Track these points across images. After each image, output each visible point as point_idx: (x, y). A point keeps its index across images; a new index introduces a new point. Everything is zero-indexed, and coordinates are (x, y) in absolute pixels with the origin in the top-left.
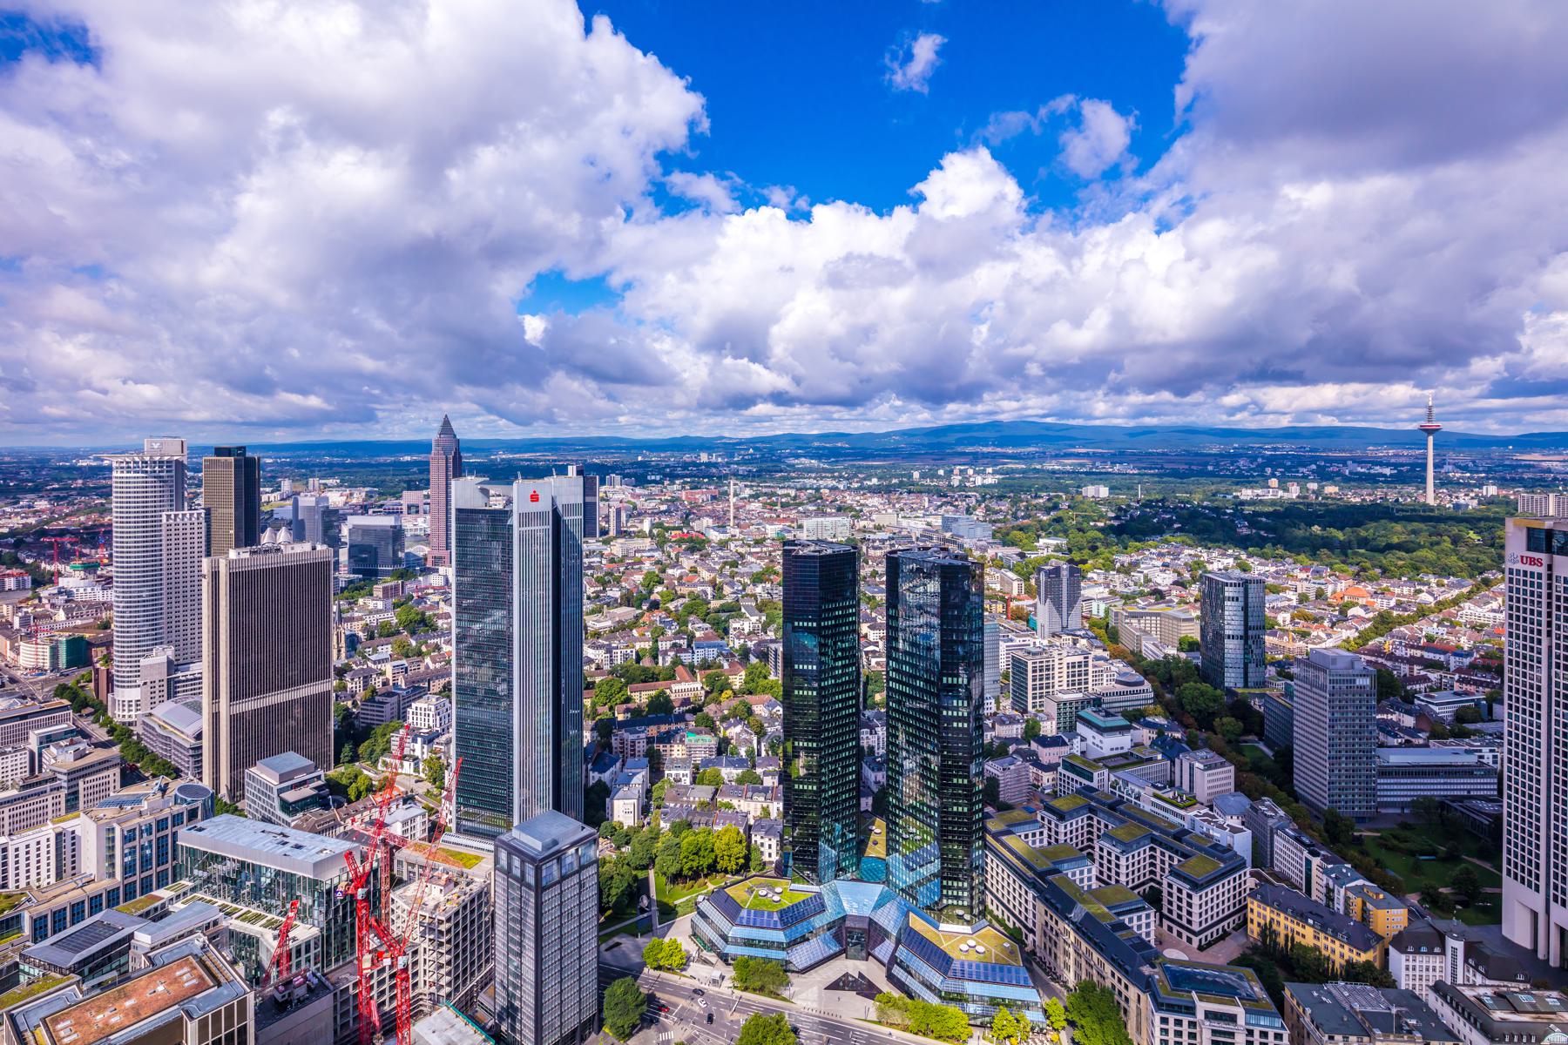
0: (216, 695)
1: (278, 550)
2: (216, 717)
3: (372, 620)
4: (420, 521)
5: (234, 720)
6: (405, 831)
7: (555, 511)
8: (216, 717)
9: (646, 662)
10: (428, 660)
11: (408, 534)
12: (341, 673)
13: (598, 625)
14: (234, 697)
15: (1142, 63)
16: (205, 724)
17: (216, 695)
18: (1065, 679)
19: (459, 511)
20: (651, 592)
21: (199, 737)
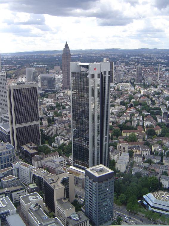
0: (12, 122)
1: (24, 83)
2: (12, 128)
3: (48, 104)
4: (59, 75)
5: (17, 129)
6: (60, 164)
7: (101, 73)
8: (12, 128)
9: (128, 124)
10: (63, 117)
11: (56, 80)
12: (41, 119)
13: (113, 111)
14: (16, 123)
15: (137, 2)
16: (10, 130)
17: (12, 122)
18: (35, 55)
19: (73, 73)
20: (130, 101)
21: (9, 133)
